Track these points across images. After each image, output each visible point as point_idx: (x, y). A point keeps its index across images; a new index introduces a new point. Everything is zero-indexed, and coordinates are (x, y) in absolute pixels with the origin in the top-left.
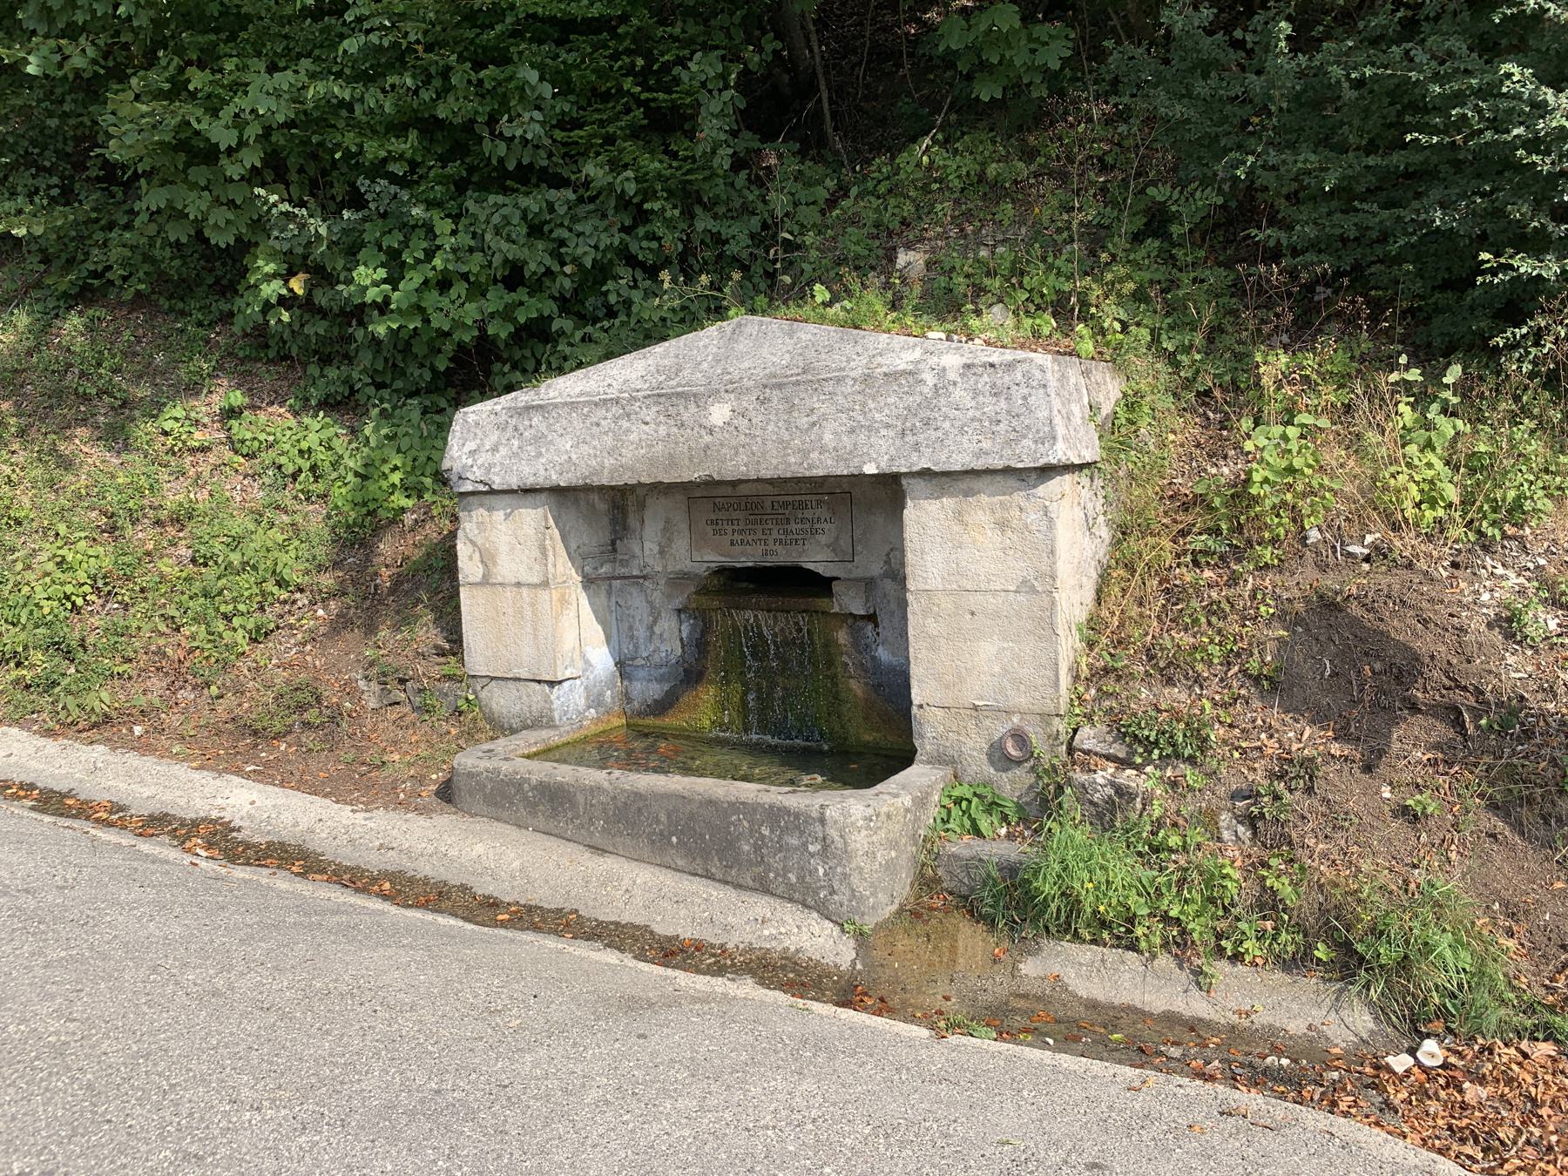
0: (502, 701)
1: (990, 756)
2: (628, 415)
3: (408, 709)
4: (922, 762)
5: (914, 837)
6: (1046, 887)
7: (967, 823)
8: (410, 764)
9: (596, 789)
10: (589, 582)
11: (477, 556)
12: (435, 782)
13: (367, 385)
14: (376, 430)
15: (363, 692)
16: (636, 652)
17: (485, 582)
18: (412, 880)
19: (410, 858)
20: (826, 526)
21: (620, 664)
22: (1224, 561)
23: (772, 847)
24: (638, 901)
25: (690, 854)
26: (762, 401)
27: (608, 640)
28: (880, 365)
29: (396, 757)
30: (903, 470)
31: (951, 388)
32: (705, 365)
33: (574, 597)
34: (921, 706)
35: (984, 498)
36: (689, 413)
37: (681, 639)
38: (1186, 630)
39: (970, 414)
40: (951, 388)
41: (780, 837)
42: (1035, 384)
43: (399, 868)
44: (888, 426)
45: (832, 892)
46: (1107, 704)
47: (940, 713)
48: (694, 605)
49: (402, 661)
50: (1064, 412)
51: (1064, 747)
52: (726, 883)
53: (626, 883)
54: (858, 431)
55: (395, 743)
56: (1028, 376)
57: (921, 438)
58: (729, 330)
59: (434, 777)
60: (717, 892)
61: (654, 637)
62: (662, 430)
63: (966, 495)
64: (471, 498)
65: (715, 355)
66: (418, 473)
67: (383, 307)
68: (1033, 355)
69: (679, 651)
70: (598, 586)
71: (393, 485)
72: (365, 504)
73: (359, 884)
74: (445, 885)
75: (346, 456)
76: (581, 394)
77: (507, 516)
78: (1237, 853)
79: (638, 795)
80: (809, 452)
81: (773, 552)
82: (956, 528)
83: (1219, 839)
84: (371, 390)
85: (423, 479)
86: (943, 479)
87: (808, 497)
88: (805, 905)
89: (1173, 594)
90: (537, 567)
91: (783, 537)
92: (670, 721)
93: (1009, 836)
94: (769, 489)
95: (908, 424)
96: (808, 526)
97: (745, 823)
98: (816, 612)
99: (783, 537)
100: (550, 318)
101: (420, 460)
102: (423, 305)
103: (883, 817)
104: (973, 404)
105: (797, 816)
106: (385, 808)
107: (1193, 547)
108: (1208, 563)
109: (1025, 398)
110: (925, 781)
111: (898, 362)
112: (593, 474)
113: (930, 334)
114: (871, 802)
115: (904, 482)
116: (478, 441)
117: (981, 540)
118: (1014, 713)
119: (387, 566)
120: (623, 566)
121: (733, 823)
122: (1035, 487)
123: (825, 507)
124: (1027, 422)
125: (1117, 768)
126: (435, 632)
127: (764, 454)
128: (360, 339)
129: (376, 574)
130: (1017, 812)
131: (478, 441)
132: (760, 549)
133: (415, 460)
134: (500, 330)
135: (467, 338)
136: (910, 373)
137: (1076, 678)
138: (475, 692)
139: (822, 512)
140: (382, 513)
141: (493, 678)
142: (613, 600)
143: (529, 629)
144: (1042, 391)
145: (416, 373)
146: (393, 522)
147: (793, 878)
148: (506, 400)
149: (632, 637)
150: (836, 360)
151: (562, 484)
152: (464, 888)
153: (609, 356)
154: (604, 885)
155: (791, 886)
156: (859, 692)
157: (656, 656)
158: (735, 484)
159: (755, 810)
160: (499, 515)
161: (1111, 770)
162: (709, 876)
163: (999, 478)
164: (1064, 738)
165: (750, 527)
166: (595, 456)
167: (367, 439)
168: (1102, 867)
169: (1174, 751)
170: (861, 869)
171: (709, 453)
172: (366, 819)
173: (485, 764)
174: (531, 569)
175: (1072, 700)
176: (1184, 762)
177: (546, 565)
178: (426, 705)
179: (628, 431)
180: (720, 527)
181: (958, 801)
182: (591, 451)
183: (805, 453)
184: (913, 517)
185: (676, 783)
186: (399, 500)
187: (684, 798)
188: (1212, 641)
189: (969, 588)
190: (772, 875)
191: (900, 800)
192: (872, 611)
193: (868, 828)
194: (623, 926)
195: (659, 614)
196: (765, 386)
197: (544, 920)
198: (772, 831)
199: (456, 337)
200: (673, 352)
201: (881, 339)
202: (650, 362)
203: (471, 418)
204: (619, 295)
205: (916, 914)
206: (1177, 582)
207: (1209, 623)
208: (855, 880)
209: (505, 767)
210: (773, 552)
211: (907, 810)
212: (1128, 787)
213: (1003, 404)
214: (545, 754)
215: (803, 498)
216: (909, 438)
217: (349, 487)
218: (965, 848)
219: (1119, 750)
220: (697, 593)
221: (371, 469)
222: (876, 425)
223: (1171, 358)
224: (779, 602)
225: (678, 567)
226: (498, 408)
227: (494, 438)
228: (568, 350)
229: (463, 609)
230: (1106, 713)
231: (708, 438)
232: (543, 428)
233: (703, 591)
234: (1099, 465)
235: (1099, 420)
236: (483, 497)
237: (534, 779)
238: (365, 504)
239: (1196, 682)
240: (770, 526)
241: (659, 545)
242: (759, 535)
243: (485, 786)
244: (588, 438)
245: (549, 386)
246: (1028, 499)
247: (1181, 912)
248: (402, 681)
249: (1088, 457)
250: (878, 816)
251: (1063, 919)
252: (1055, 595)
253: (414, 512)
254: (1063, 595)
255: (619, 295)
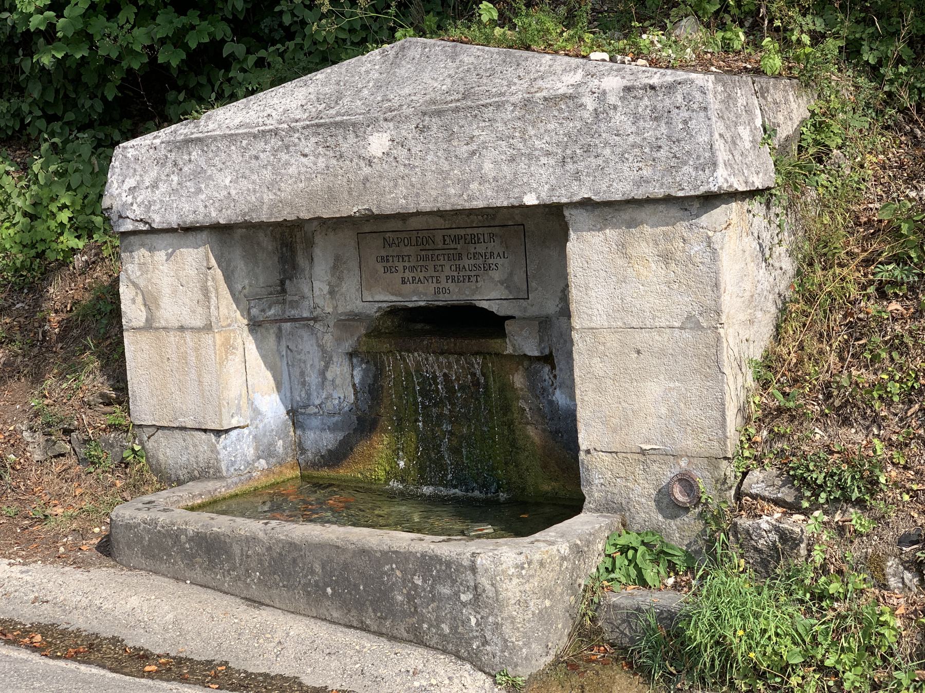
0: (168, 450)
1: (658, 502)
2: (287, 147)
3: (72, 461)
4: (590, 510)
5: (572, 587)
6: (698, 635)
7: (633, 573)
8: (72, 518)
9: (252, 540)
10: (255, 326)
11: (139, 299)
12: (97, 535)
13: (39, 118)
14: (44, 167)
15: (28, 444)
16: (309, 399)
17: (149, 326)
18: (64, 633)
19: (64, 611)
20: (500, 261)
21: (293, 413)
22: (914, 292)
23: (425, 597)
24: (290, 653)
25: (345, 606)
26: (422, 129)
27: (279, 386)
28: (540, 89)
29: (59, 510)
30: (564, 200)
31: (611, 112)
32: (366, 92)
33: (239, 341)
34: (588, 452)
35: (647, 229)
36: (347, 144)
37: (354, 385)
38: (866, 367)
39: (631, 139)
40: (611, 112)
41: (433, 587)
42: (695, 106)
43: (53, 621)
44: (548, 154)
45: (485, 643)
46: (778, 445)
47: (607, 458)
48: (364, 348)
49: (67, 411)
50: (728, 136)
51: (733, 492)
52: (381, 634)
53: (279, 635)
54: (518, 160)
55: (59, 496)
56: (688, 98)
57: (581, 166)
58: (392, 53)
59: (97, 530)
60: (369, 644)
61: (327, 383)
62: (321, 162)
63: (629, 226)
64: (132, 239)
65: (377, 80)
66: (88, 212)
67: (49, 35)
68: (693, 76)
69: (352, 398)
70: (267, 329)
71: (62, 224)
72: (33, 246)
73: (10, 636)
74: (97, 637)
75: (14, 196)
76: (240, 126)
77: (169, 256)
78: (902, 601)
79: (293, 546)
80: (469, 183)
81: (446, 291)
82: (620, 262)
83: (885, 587)
84: (42, 124)
85: (94, 218)
86: (607, 209)
87: (480, 230)
88: (459, 657)
89: (857, 329)
90: (200, 310)
91: (455, 274)
92: (343, 472)
93: (676, 587)
94: (440, 223)
95: (569, 152)
96: (480, 261)
97: (398, 573)
98: (490, 354)
99: (455, 274)
100: (223, 42)
101: (90, 198)
102: (90, 31)
103: (536, 565)
104: (634, 129)
105: (448, 564)
106: (43, 562)
107: (878, 277)
108: (896, 295)
109: (685, 122)
110: (587, 528)
111: (559, 85)
112: (252, 210)
113: (593, 56)
114: (524, 550)
115: (566, 213)
116: (138, 178)
117: (645, 273)
118: (681, 456)
119: (56, 312)
120: (293, 308)
121: (386, 573)
122: (698, 216)
123: (498, 241)
124: (687, 148)
125: (784, 513)
126: (101, 380)
127: (424, 184)
128: (27, 70)
129: (44, 319)
130: (685, 561)
131: (138, 178)
132: (431, 288)
133: (85, 197)
134: (171, 58)
135: (136, 66)
136: (571, 97)
137: (747, 419)
138: (141, 443)
139: (495, 246)
140: (51, 256)
141: (159, 428)
142: (284, 343)
143: (193, 375)
144: (702, 114)
145: (88, 103)
146: (64, 264)
147: (446, 628)
148: (165, 133)
149: (304, 384)
150: (497, 84)
151: (222, 222)
152: (115, 641)
153: (279, 81)
154: (257, 637)
155: (443, 636)
156: (537, 440)
157: (329, 403)
158: (403, 217)
159: (407, 559)
160: (161, 255)
161: (777, 515)
162: (365, 628)
163: (661, 208)
164: (733, 482)
165: (421, 263)
166: (254, 191)
167: (36, 175)
168: (757, 616)
169: (843, 495)
170: (513, 620)
171: (368, 185)
172: (22, 572)
173: (144, 515)
174: (194, 312)
175: (741, 442)
176: (853, 506)
177: (209, 308)
178: (91, 456)
179: (287, 164)
180: (390, 264)
181: (624, 550)
182: (251, 187)
183: (464, 184)
184: (576, 250)
185: (333, 533)
186: (69, 241)
187: (338, 547)
188: (892, 378)
189: (634, 324)
190: (425, 626)
191: (555, 548)
192: (547, 352)
193: (520, 576)
194: (272, 678)
195: (331, 358)
196: (424, 114)
197: (193, 671)
198: (424, 581)
199: (124, 64)
200: (334, 78)
201: (543, 61)
202: (311, 90)
203: (131, 153)
204: (293, 15)
205: (572, 666)
206: (862, 316)
207: (892, 360)
208: (507, 629)
209: (163, 518)
210: (446, 291)
211: (564, 558)
212: (792, 532)
213: (663, 129)
214: (212, 505)
215: (475, 231)
216: (570, 166)
217: (17, 228)
218: (627, 598)
219: (787, 494)
220: (368, 335)
221: (39, 209)
222: (537, 153)
223: (874, 72)
224: (446, 344)
225: (349, 308)
226: (157, 141)
227: (153, 174)
228: (240, 76)
229: (128, 355)
230: (777, 456)
231: (367, 170)
232: (203, 163)
233: (375, 333)
234: (773, 191)
235: (775, 143)
236: (143, 237)
237: (191, 529)
238: (33, 246)
239: (874, 422)
240: (442, 262)
241: (329, 284)
242: (431, 272)
243: (142, 538)
244: (247, 172)
245: (209, 118)
246: (691, 229)
247: (838, 661)
248: (67, 432)
249: (758, 182)
250: (530, 563)
251: (717, 667)
252: (721, 331)
253: (85, 253)
254: (731, 331)
255: (293, 15)
